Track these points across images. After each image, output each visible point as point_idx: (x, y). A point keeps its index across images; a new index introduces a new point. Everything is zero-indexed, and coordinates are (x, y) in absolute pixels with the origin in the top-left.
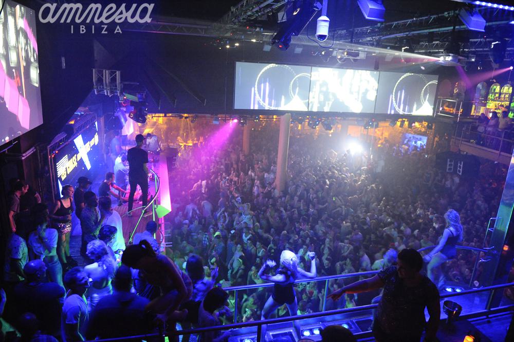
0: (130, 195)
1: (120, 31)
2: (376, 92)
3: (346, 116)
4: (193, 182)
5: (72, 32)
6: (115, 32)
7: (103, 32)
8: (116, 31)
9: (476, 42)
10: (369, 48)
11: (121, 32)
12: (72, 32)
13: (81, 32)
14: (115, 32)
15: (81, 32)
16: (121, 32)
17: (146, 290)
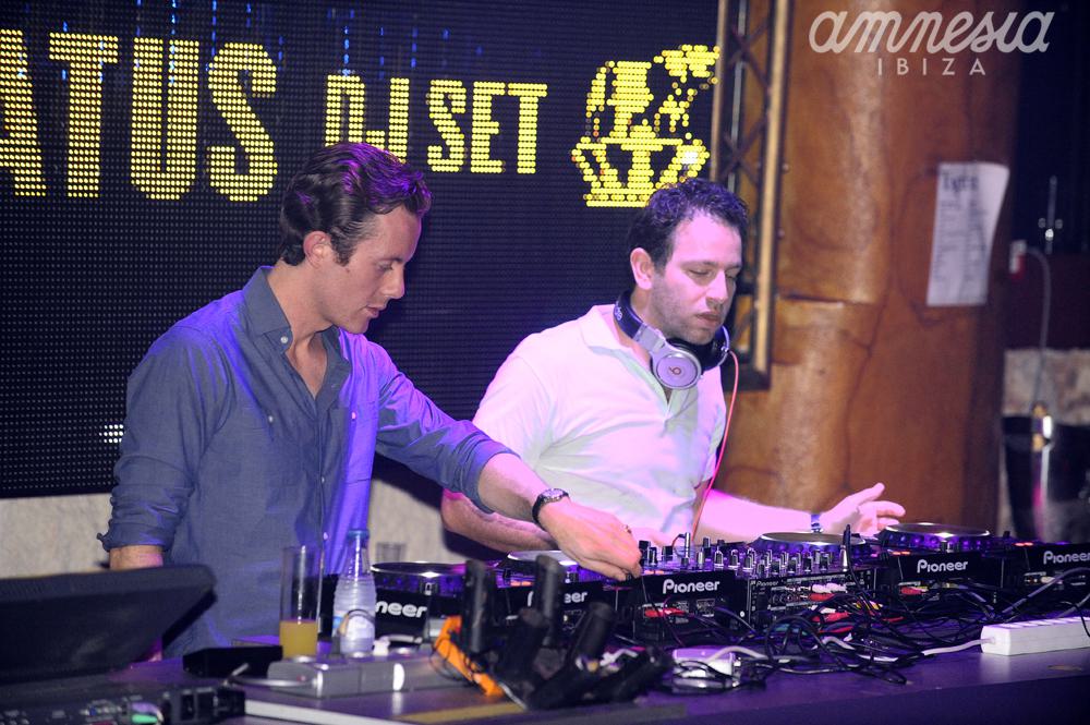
1: (982, 70)
7: (946, 73)
8: (973, 70)
11: (984, 73)
13: (899, 73)
14: (971, 73)
15: (899, 73)
16: (984, 73)
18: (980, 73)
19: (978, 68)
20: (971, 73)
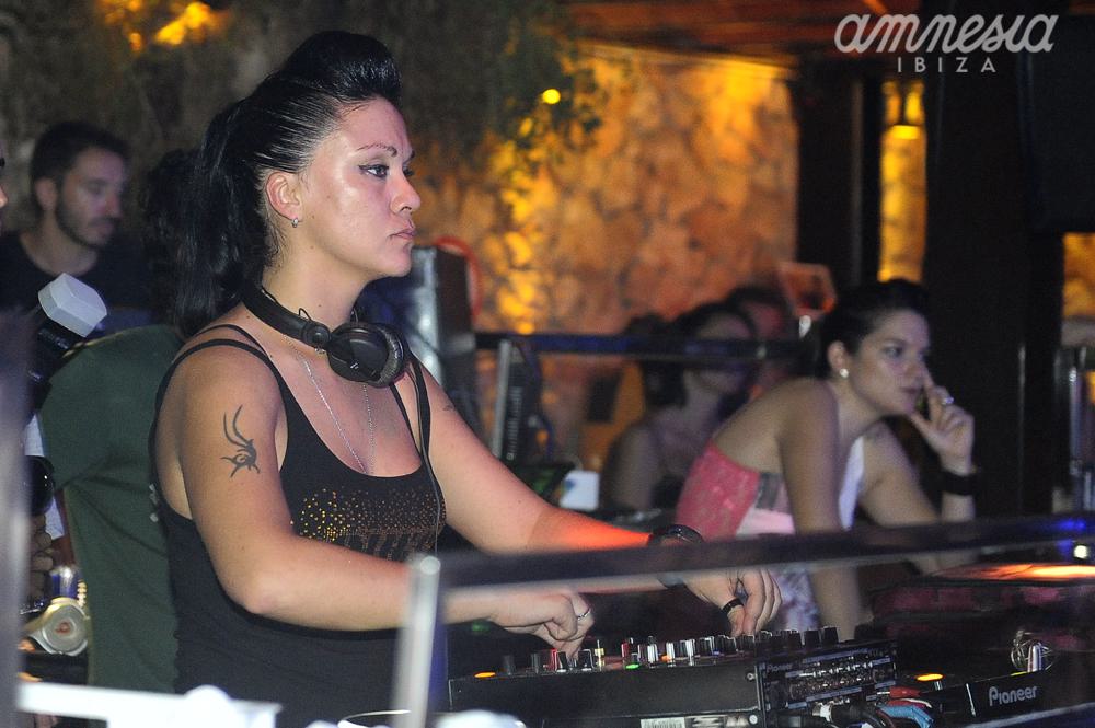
1: (992, 69)
7: (959, 70)
8: (984, 69)
11: (994, 71)
13: (917, 70)
14: (983, 71)
15: (917, 70)
16: (994, 71)
19: (988, 66)
20: (983, 71)
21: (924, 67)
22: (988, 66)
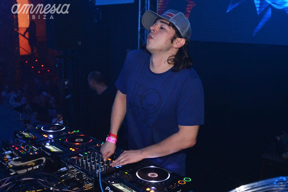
0: (179, 50)
1: (53, 18)
2: (153, 62)
3: (187, 36)
4: (47, 158)
5: (39, 18)
6: (50, 19)
7: (44, 18)
8: (51, 18)
9: (141, 40)
10: (23, 171)
11: (53, 19)
12: (39, 18)
13: (33, 19)
14: (50, 19)
15: (33, 19)
16: (53, 19)
17: (25, 171)
18: (52, 19)
19: (52, 17)
21: (35, 18)
22: (52, 17)
